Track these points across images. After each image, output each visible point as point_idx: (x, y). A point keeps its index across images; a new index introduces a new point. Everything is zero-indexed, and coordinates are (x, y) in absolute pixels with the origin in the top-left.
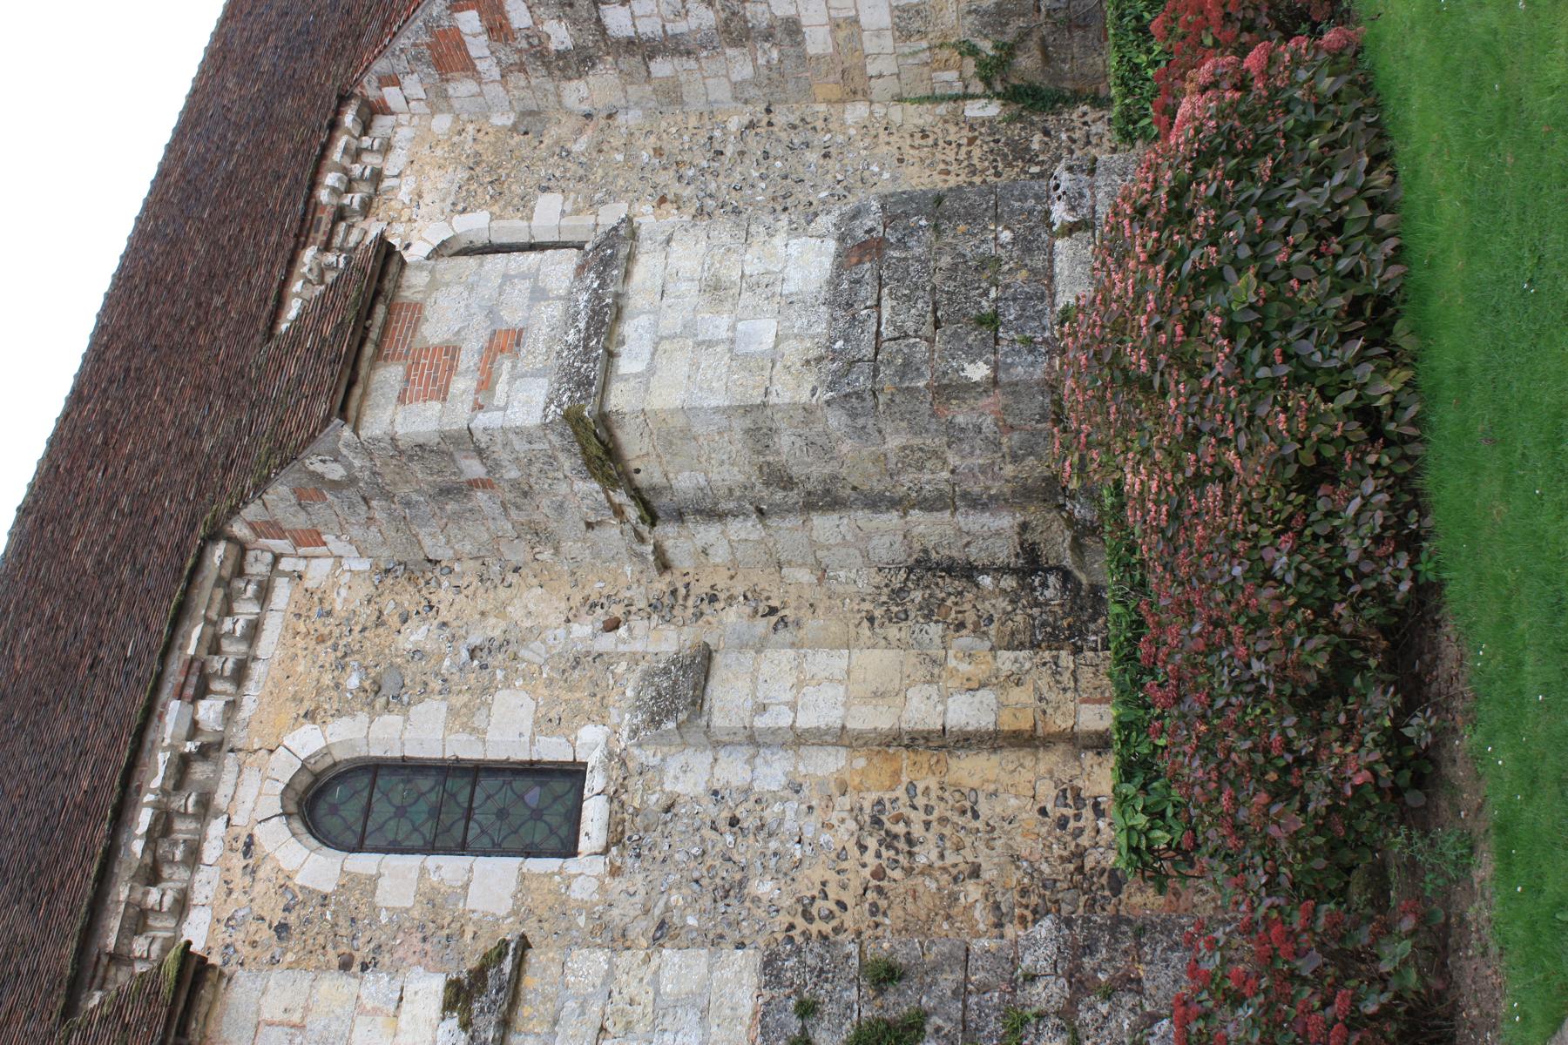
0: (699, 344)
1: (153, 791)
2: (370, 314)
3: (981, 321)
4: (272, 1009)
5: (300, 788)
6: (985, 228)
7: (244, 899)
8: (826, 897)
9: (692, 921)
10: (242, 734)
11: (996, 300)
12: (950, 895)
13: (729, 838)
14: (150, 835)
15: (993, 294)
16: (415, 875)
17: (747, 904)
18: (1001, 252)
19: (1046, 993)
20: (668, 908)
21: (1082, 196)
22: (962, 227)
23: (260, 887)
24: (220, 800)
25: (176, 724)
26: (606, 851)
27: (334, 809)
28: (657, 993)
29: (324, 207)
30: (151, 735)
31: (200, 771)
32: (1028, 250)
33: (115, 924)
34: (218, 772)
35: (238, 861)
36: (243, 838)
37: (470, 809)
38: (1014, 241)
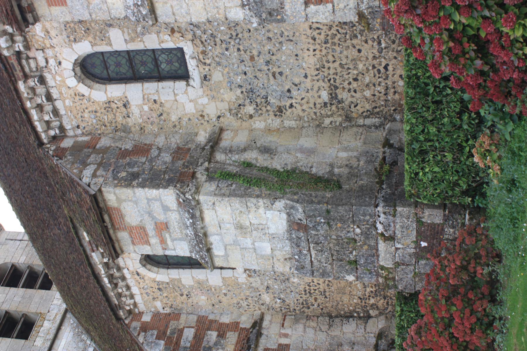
0: (242, 249)
2: (104, 221)
3: (350, 262)
6: (349, 226)
11: (356, 256)
15: (354, 253)
18: (356, 237)
20: (268, 284)
21: (389, 225)
22: (339, 225)
23: (147, 282)
25: (98, 258)
29: (9, 57)
30: (92, 262)
32: (367, 238)
38: (362, 233)
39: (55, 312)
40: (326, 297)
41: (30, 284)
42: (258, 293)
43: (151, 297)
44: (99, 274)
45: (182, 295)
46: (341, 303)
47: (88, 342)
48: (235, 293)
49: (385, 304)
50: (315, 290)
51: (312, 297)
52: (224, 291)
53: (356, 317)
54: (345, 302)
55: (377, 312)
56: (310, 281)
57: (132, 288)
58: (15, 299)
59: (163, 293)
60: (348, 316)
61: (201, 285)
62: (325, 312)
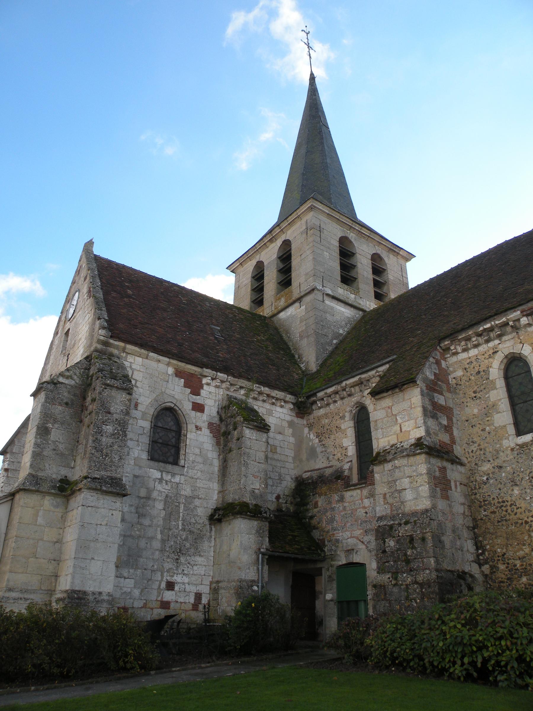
1: (495, 323)
4: (414, 400)
5: (515, 355)
7: (483, 359)
8: (517, 509)
9: (503, 474)
10: (523, 332)
12: (524, 543)
13: (527, 478)
14: (485, 330)
16: (499, 398)
17: (511, 488)
19: (420, 579)
20: (506, 467)
23: (486, 361)
24: (505, 338)
26: (517, 445)
27: (516, 366)
28: (419, 486)
30: (508, 312)
31: (509, 329)
33: (464, 335)
34: (511, 333)
35: (491, 351)
36: (497, 350)
37: (526, 402)
39: (361, 303)
40: (499, 522)
41: (377, 284)
42: (491, 459)
43: (467, 366)
44: (495, 319)
45: (475, 392)
46: (494, 536)
47: (346, 329)
48: (488, 438)
49: (500, 579)
50: (506, 511)
51: (496, 508)
52: (488, 428)
53: (478, 552)
54: (495, 541)
55: (487, 572)
56: (518, 506)
57: (476, 350)
58: (365, 272)
59: (474, 376)
60: (478, 545)
61: (490, 410)
62: (478, 522)
